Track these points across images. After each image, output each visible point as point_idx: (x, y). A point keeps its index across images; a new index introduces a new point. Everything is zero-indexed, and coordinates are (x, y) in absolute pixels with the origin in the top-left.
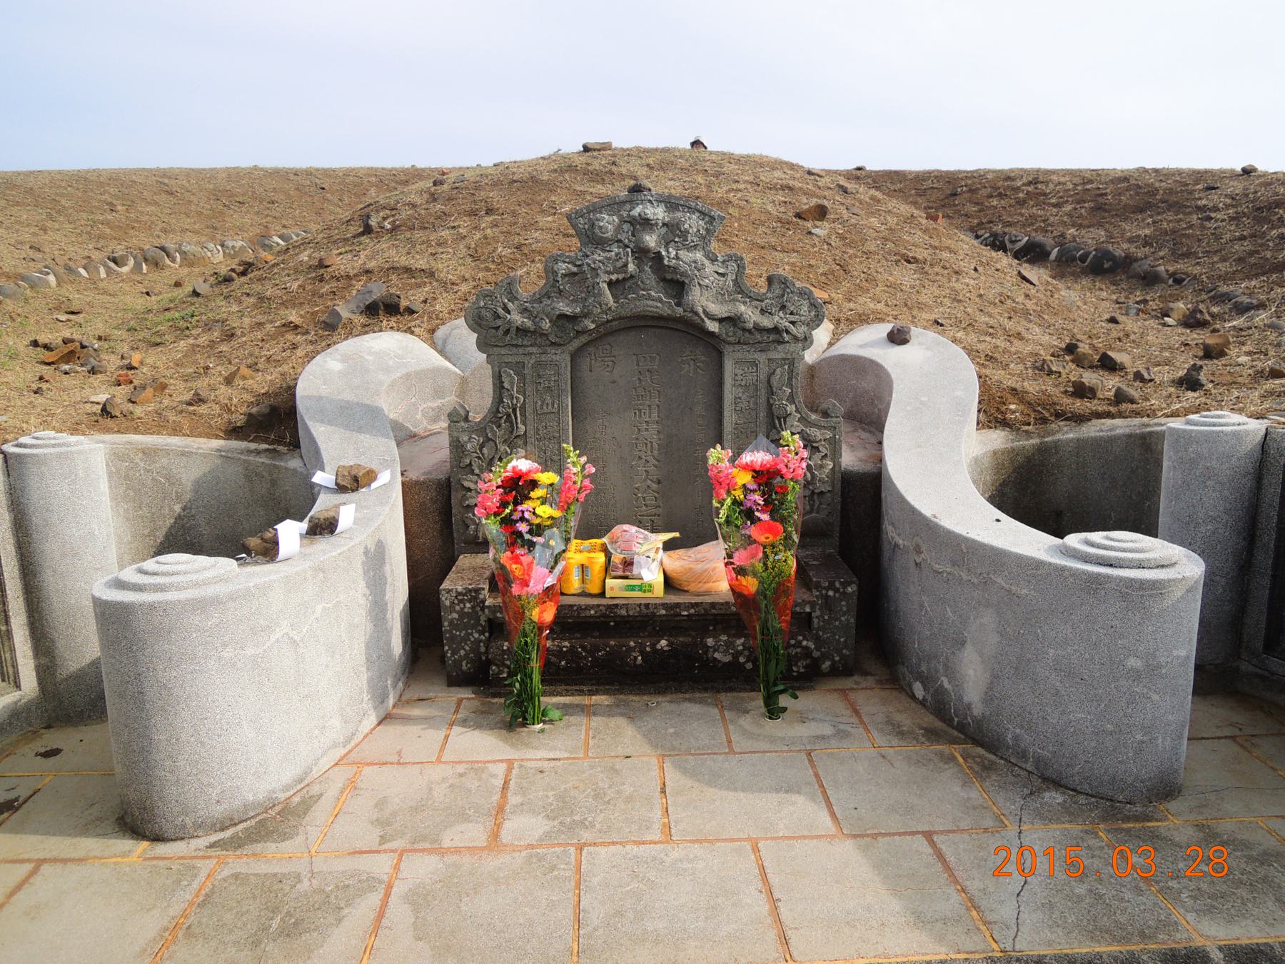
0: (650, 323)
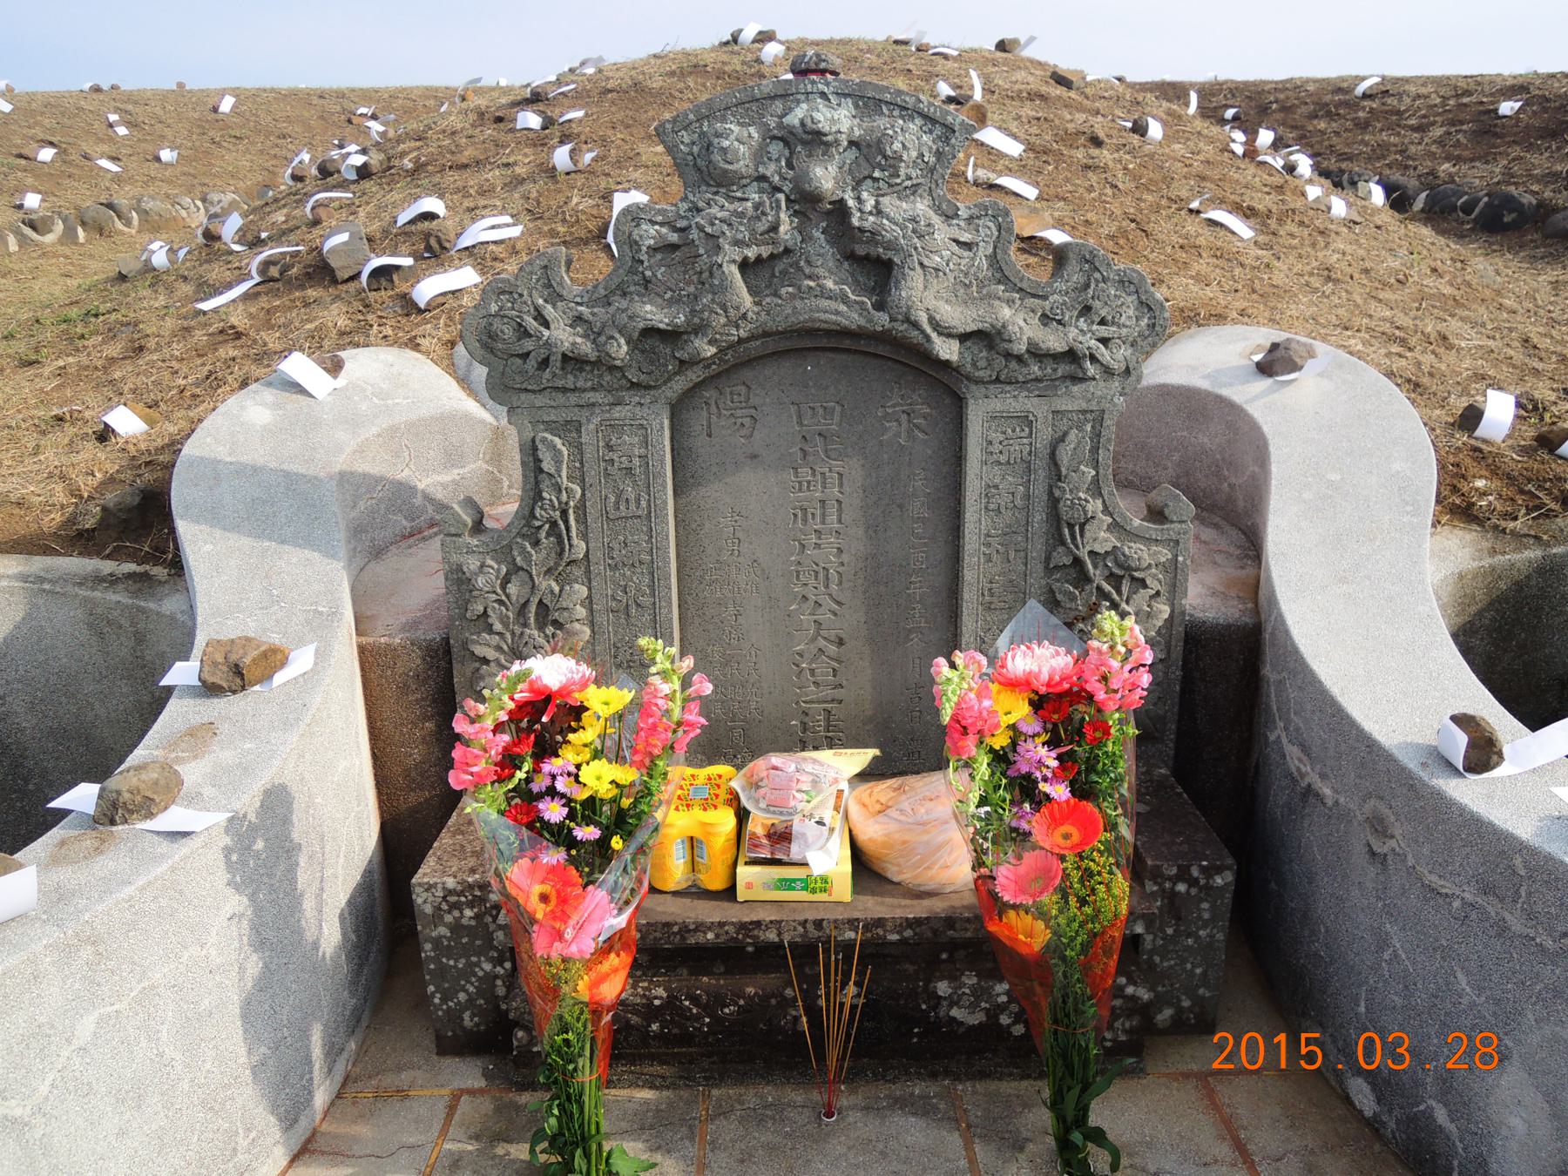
0: (824, 343)
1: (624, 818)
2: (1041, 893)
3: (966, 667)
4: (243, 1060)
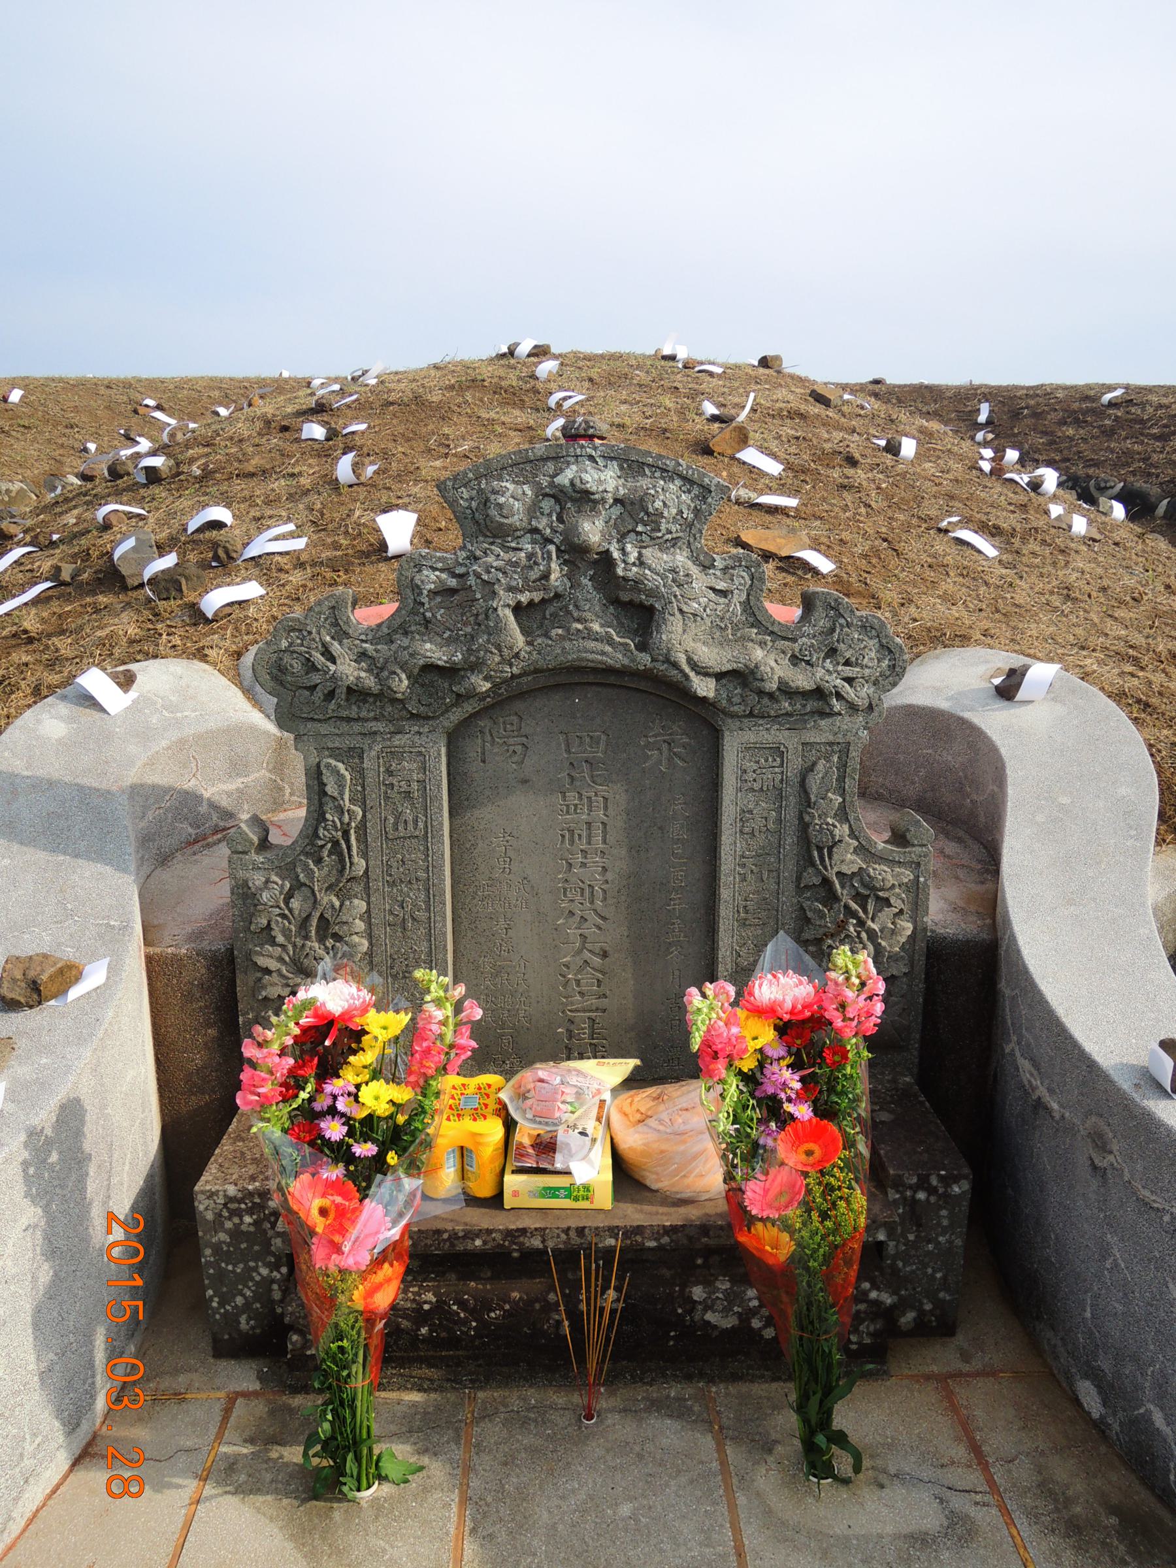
0: (591, 679)
1: (400, 1137)
2: (787, 1207)
3: (716, 995)
4: (32, 1367)
